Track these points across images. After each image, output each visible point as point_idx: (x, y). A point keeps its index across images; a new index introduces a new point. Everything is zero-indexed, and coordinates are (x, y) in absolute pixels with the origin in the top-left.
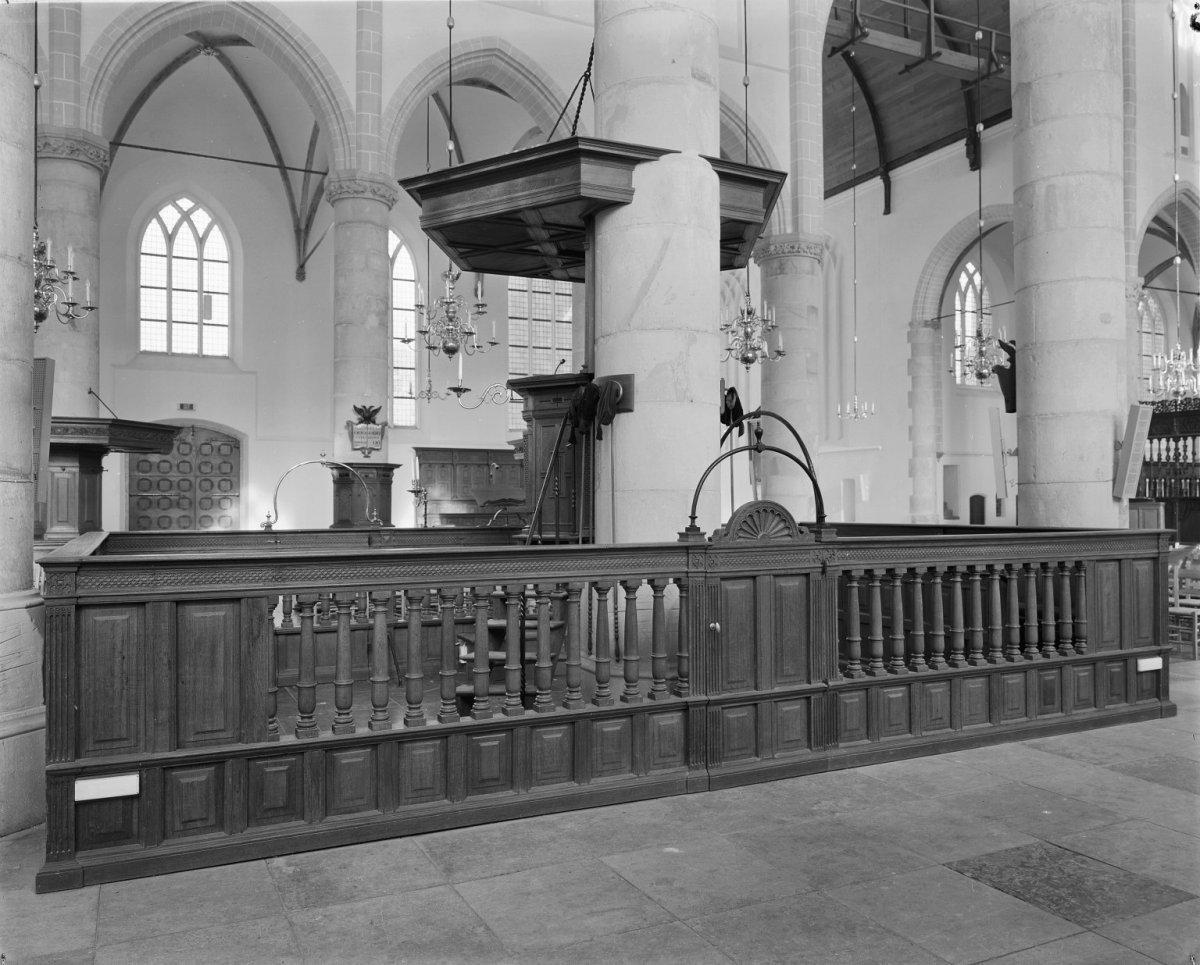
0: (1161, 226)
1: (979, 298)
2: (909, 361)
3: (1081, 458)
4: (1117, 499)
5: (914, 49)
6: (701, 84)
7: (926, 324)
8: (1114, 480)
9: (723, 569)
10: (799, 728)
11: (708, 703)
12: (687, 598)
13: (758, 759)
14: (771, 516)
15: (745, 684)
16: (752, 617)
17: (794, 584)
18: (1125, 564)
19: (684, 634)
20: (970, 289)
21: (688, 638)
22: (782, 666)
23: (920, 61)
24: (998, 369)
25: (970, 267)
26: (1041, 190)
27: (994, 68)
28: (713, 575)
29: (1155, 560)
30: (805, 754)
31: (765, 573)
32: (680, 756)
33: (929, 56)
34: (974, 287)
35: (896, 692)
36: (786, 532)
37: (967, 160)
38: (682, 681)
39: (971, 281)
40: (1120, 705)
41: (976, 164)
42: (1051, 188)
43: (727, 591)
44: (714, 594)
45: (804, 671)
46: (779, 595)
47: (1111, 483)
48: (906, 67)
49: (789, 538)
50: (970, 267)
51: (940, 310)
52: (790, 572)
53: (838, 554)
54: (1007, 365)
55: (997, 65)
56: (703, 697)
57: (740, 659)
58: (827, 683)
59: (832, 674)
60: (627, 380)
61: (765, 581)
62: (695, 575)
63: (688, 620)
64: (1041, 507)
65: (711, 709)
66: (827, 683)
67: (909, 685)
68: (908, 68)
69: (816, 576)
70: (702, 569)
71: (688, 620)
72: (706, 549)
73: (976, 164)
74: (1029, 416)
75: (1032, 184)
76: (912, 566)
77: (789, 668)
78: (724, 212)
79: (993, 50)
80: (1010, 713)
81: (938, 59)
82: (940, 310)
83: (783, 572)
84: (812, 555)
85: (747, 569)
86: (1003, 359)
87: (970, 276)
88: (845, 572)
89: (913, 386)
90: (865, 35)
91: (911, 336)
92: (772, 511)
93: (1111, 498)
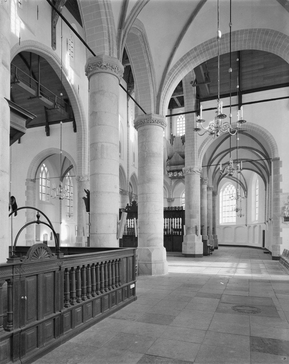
0: (212, 160)
1: (46, 175)
2: (26, 192)
3: (109, 227)
4: (117, 239)
5: (33, 92)
6: (5, 68)
7: (31, 180)
8: (117, 233)
9: (27, 273)
10: (51, 332)
11: (21, 331)
12: (12, 287)
13: (38, 348)
14: (43, 249)
15: (33, 319)
16: (36, 291)
17: (50, 275)
18: (128, 258)
19: (11, 303)
20: (44, 172)
21: (13, 305)
22: (46, 308)
23: (35, 97)
24: (84, 198)
25: (44, 165)
26: (99, 145)
27: (56, 107)
28: (23, 276)
29: (133, 256)
30: (54, 341)
31: (41, 272)
32: (9, 358)
33: (37, 96)
34: (45, 171)
35: (79, 309)
36: (48, 255)
37: (46, 133)
38: (9, 324)
39: (44, 169)
40: (127, 299)
41: (48, 134)
42: (102, 146)
43: (27, 282)
44: (23, 283)
45: (52, 309)
46: (45, 280)
47: (116, 234)
48: (30, 97)
49: (49, 258)
50: (44, 165)
51: (35, 177)
52: (50, 271)
53: (64, 262)
54: (86, 197)
55: (57, 106)
56: (19, 329)
57: (31, 309)
58: (61, 312)
59: (62, 308)
60: (282, 189)
61: (41, 276)
62: (16, 277)
63: (13, 298)
64: (98, 241)
65: (22, 333)
66: (61, 312)
67: (82, 306)
68: (31, 98)
69: (57, 272)
70: (19, 274)
71: (13, 298)
72: (20, 265)
73: (48, 134)
74: (95, 213)
75: (97, 143)
76: (84, 264)
77: (48, 309)
78: (12, 125)
79: (56, 101)
80: (106, 308)
81: (40, 98)
82: (35, 177)
83: (47, 271)
84: (56, 264)
85: (35, 272)
86: (85, 195)
87: (44, 168)
88: (65, 269)
89: (27, 199)
90: (19, 82)
91: (26, 184)
92: (44, 248)
93: (116, 238)
